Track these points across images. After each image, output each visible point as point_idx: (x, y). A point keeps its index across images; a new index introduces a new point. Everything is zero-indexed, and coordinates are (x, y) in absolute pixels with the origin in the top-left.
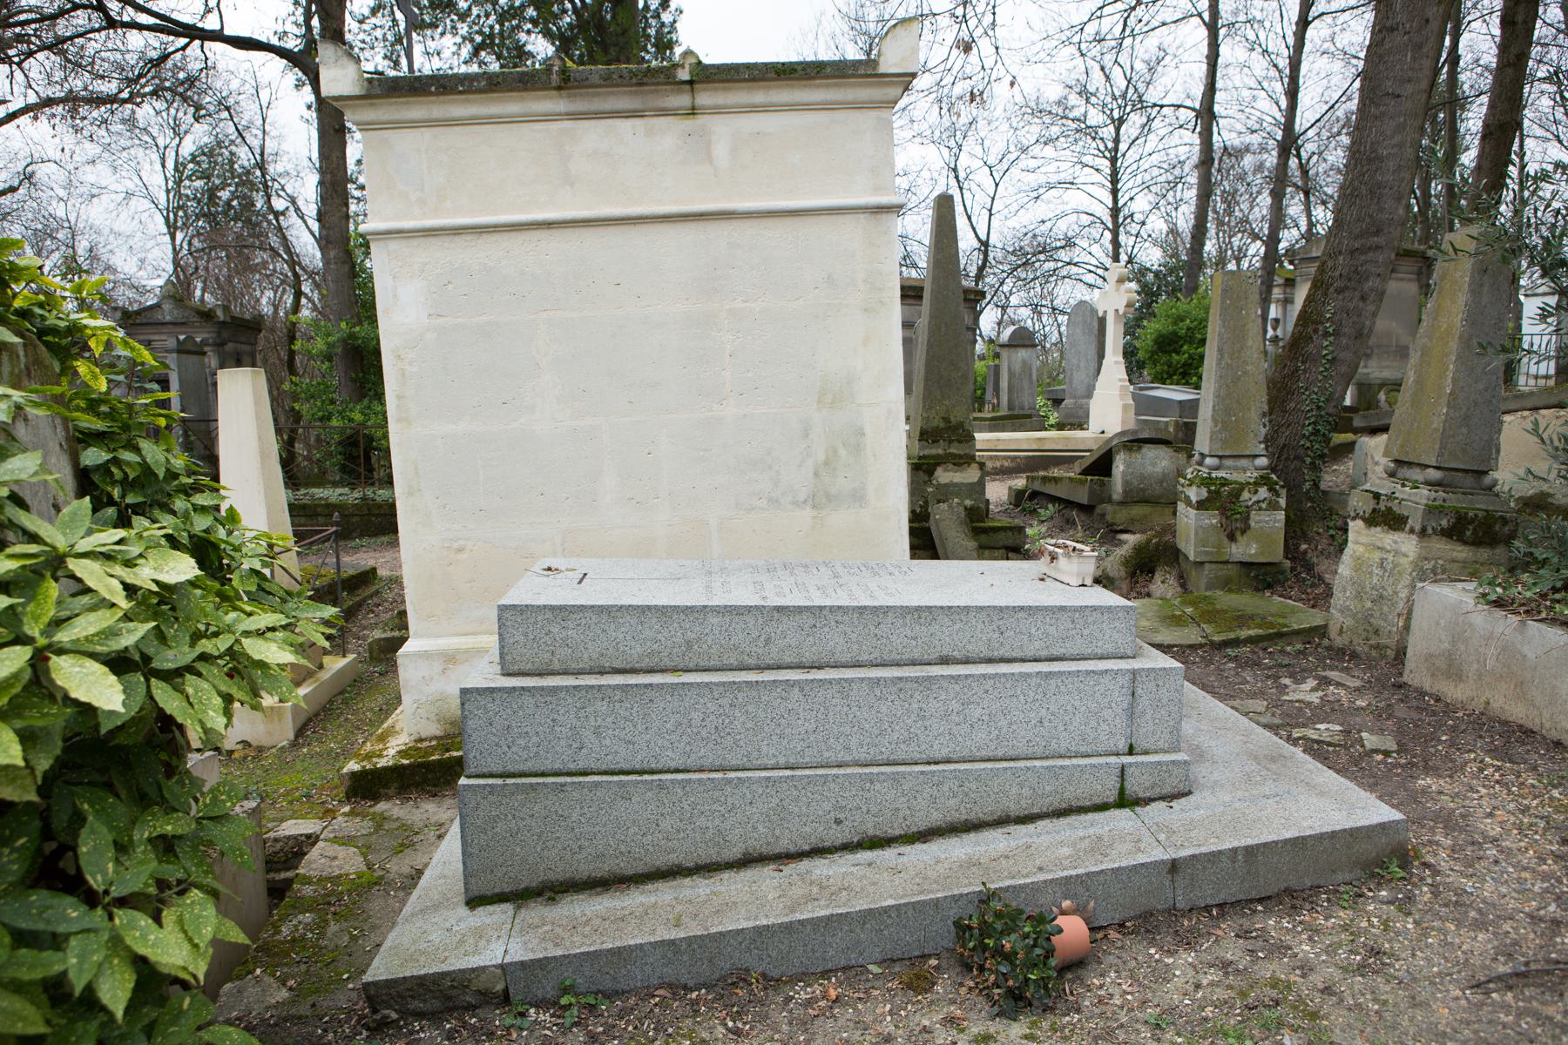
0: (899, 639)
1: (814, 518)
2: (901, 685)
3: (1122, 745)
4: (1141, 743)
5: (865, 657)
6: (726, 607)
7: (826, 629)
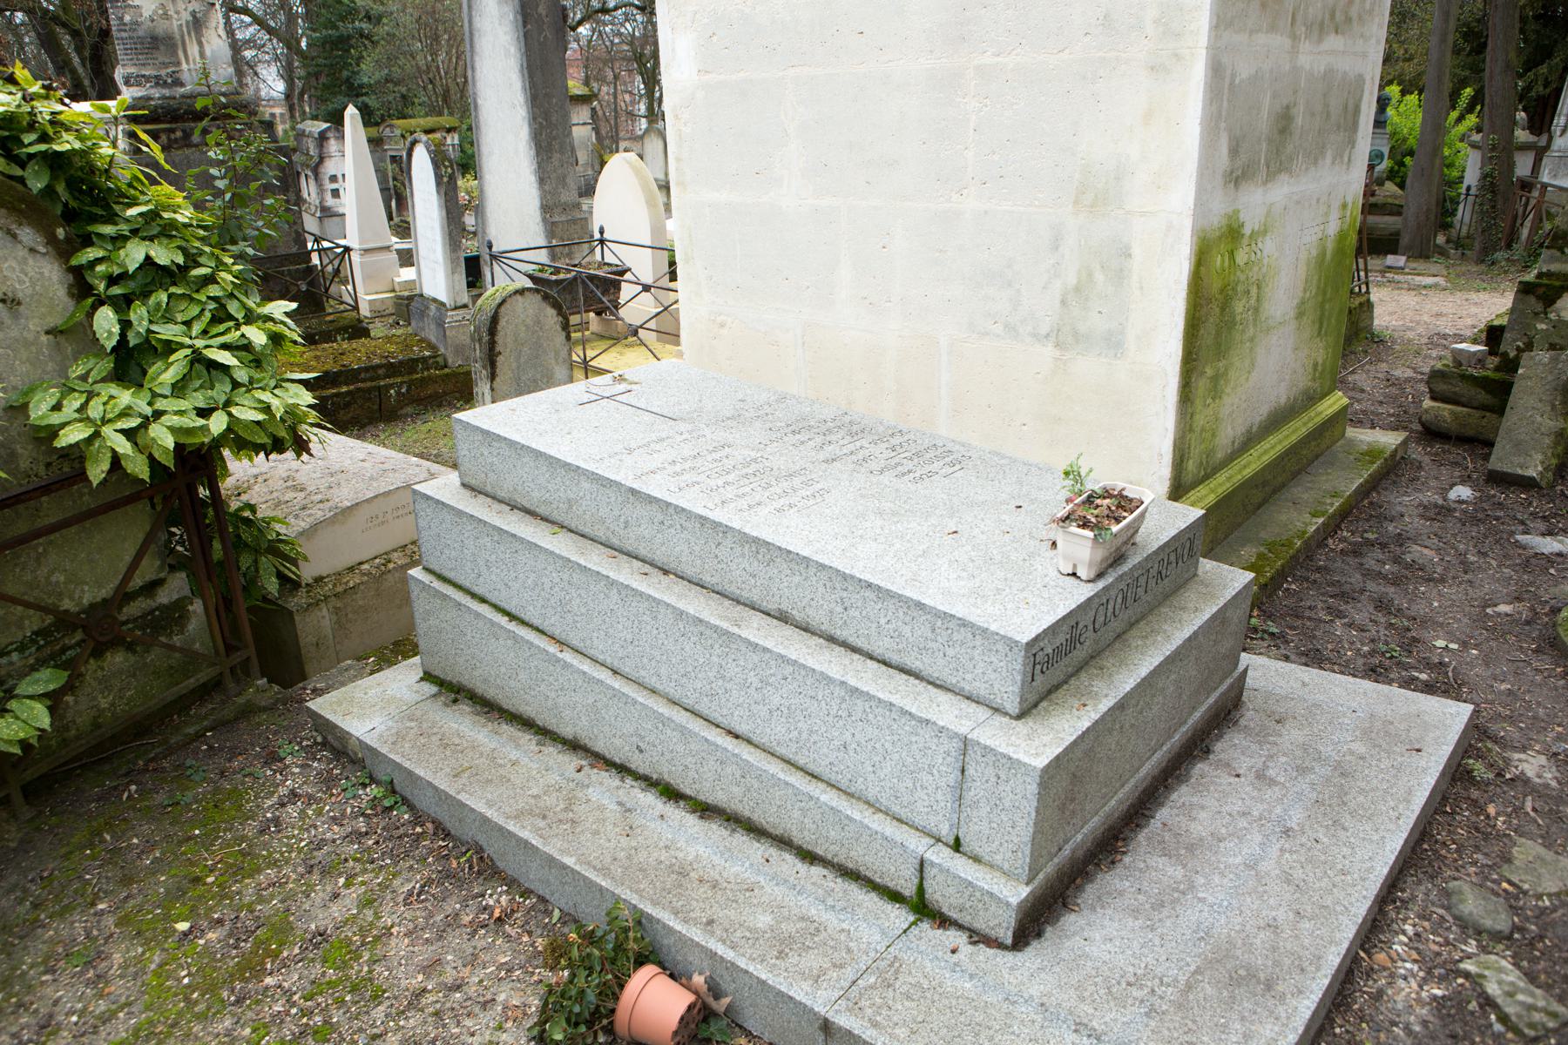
0: (738, 572)
1: (1056, 359)
2: (702, 629)
3: (945, 831)
4: (969, 843)
5: (707, 578)
6: (593, 473)
7: (673, 530)
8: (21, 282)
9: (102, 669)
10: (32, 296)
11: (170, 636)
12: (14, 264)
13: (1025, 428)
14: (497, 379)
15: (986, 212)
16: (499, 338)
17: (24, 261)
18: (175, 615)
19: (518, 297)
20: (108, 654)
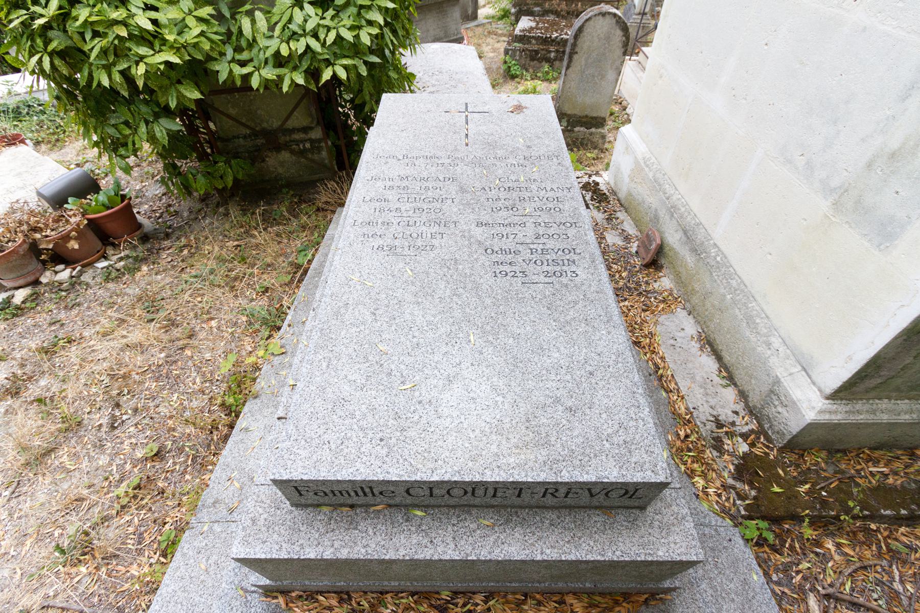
13: (769, 257)
14: (570, 69)
16: (579, 42)
19: (600, 17)
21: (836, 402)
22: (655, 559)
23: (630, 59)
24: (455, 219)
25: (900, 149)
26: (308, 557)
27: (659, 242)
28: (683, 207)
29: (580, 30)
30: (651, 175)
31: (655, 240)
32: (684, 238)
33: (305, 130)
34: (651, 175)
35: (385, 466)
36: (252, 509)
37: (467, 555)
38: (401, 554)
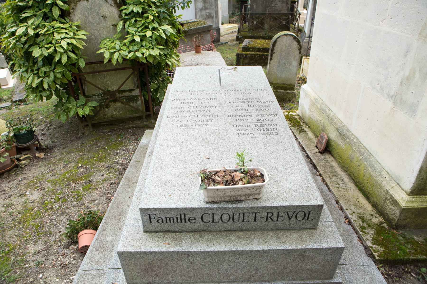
8: (107, 13)
9: (115, 105)
10: (110, 16)
11: (133, 103)
12: (106, 8)
14: (272, 61)
15: (388, 32)
16: (275, 48)
17: (109, 7)
18: (134, 99)
19: (285, 36)
20: (117, 103)
21: (414, 196)
22: (322, 247)
23: (306, 58)
24: (217, 114)
25: (409, 75)
26: (154, 251)
27: (326, 138)
28: (336, 119)
29: (275, 42)
30: (319, 106)
31: (325, 138)
32: (338, 134)
33: (131, 91)
34: (319, 106)
35: (191, 203)
36: (125, 234)
37: (231, 249)
38: (199, 249)
